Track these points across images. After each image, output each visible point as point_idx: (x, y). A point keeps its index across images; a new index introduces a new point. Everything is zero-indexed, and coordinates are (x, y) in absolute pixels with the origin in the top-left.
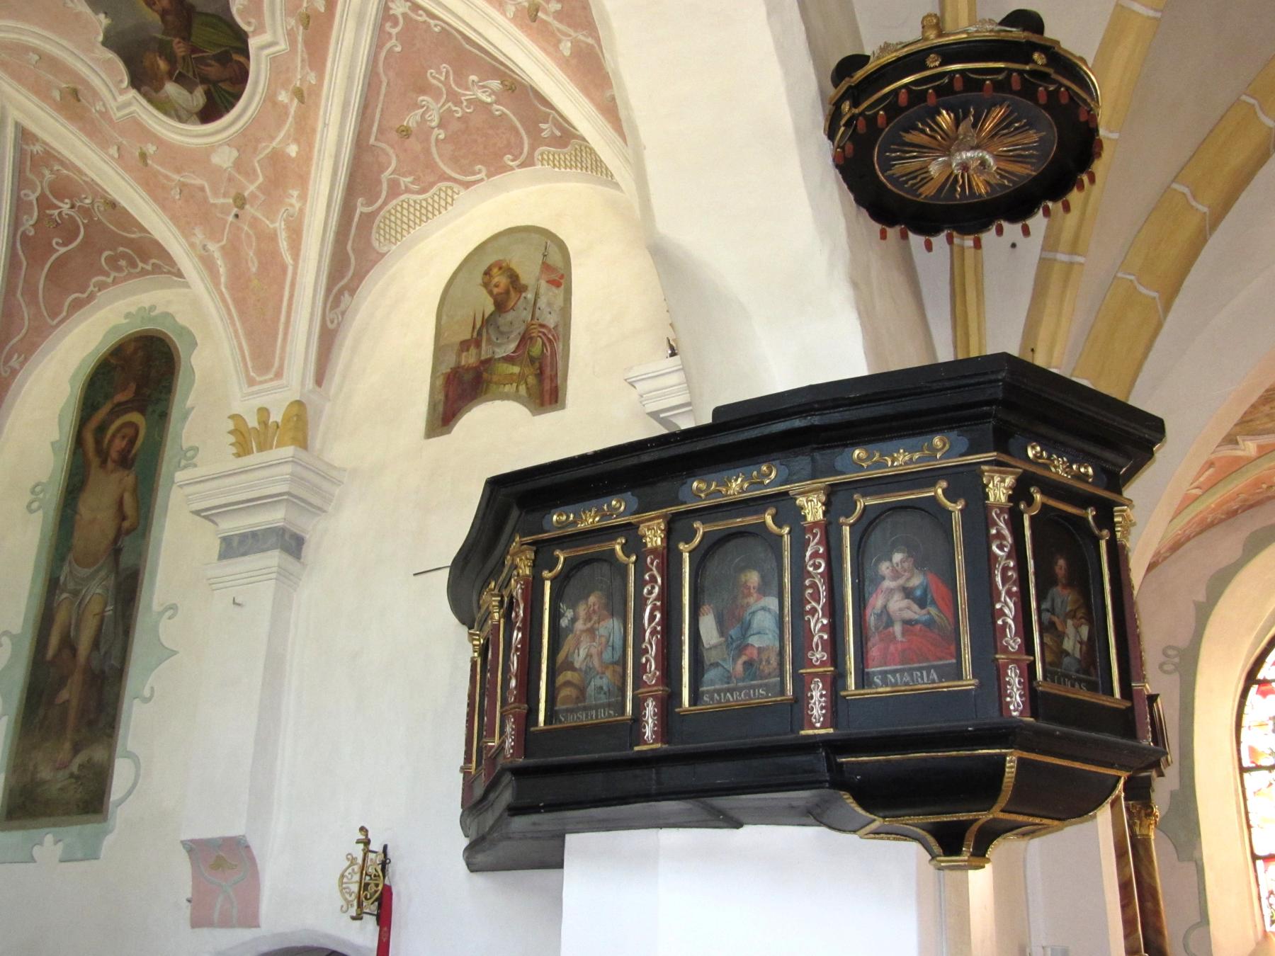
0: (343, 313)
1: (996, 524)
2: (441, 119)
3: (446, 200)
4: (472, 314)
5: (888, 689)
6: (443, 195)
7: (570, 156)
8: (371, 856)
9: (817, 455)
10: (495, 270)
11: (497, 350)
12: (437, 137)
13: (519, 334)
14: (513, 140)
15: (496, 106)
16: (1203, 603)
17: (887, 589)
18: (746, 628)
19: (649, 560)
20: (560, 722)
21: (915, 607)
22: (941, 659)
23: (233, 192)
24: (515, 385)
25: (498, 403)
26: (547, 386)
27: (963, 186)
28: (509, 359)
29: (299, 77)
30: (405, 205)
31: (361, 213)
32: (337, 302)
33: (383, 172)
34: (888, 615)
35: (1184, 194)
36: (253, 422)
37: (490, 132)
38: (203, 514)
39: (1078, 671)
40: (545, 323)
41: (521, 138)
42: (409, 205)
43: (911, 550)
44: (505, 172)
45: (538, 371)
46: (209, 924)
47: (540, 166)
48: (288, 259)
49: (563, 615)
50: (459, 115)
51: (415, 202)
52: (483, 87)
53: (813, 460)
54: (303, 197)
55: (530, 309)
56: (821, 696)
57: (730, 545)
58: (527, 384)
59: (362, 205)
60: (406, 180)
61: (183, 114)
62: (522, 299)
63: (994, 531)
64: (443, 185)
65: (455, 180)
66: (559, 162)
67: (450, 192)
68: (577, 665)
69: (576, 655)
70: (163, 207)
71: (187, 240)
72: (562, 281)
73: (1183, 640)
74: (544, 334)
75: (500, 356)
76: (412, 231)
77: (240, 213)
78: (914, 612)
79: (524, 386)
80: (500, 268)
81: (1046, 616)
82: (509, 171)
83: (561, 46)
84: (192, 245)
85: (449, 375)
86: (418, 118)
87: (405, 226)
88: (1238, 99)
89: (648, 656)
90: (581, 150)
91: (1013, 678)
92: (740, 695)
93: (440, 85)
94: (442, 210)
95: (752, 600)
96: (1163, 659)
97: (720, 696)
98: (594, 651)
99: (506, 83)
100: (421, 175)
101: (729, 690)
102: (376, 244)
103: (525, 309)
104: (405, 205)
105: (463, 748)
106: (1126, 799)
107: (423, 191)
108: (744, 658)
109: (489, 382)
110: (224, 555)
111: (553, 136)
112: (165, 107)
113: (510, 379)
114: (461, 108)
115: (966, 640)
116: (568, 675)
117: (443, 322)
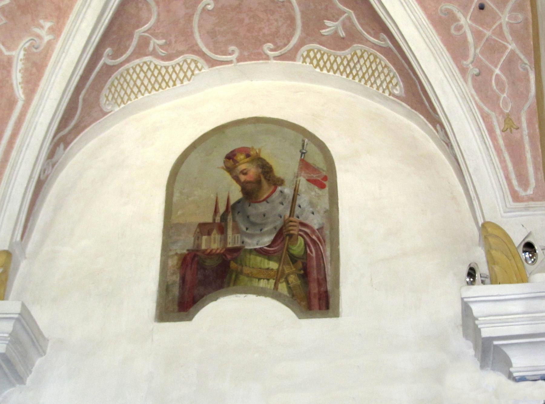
4: (213, 196)
6: (185, 67)
11: (247, 240)
12: (206, 5)
13: (275, 228)
14: (283, 30)
25: (251, 297)
26: (314, 289)
28: (261, 252)
30: (145, 68)
33: (138, 27)
41: (294, 30)
44: (258, 60)
45: (302, 272)
47: (301, 63)
48: (20, 93)
51: (156, 66)
54: (56, 31)
60: (155, 42)
62: (277, 194)
64: (190, 57)
67: (193, 66)
75: (252, 247)
76: (140, 97)
79: (284, 285)
80: (248, 156)
82: (265, 59)
87: (136, 90)
100: (173, 41)
102: (103, 100)
103: (282, 204)
104: (145, 68)
107: (169, 58)
109: (239, 273)
113: (267, 274)
117: (175, 199)
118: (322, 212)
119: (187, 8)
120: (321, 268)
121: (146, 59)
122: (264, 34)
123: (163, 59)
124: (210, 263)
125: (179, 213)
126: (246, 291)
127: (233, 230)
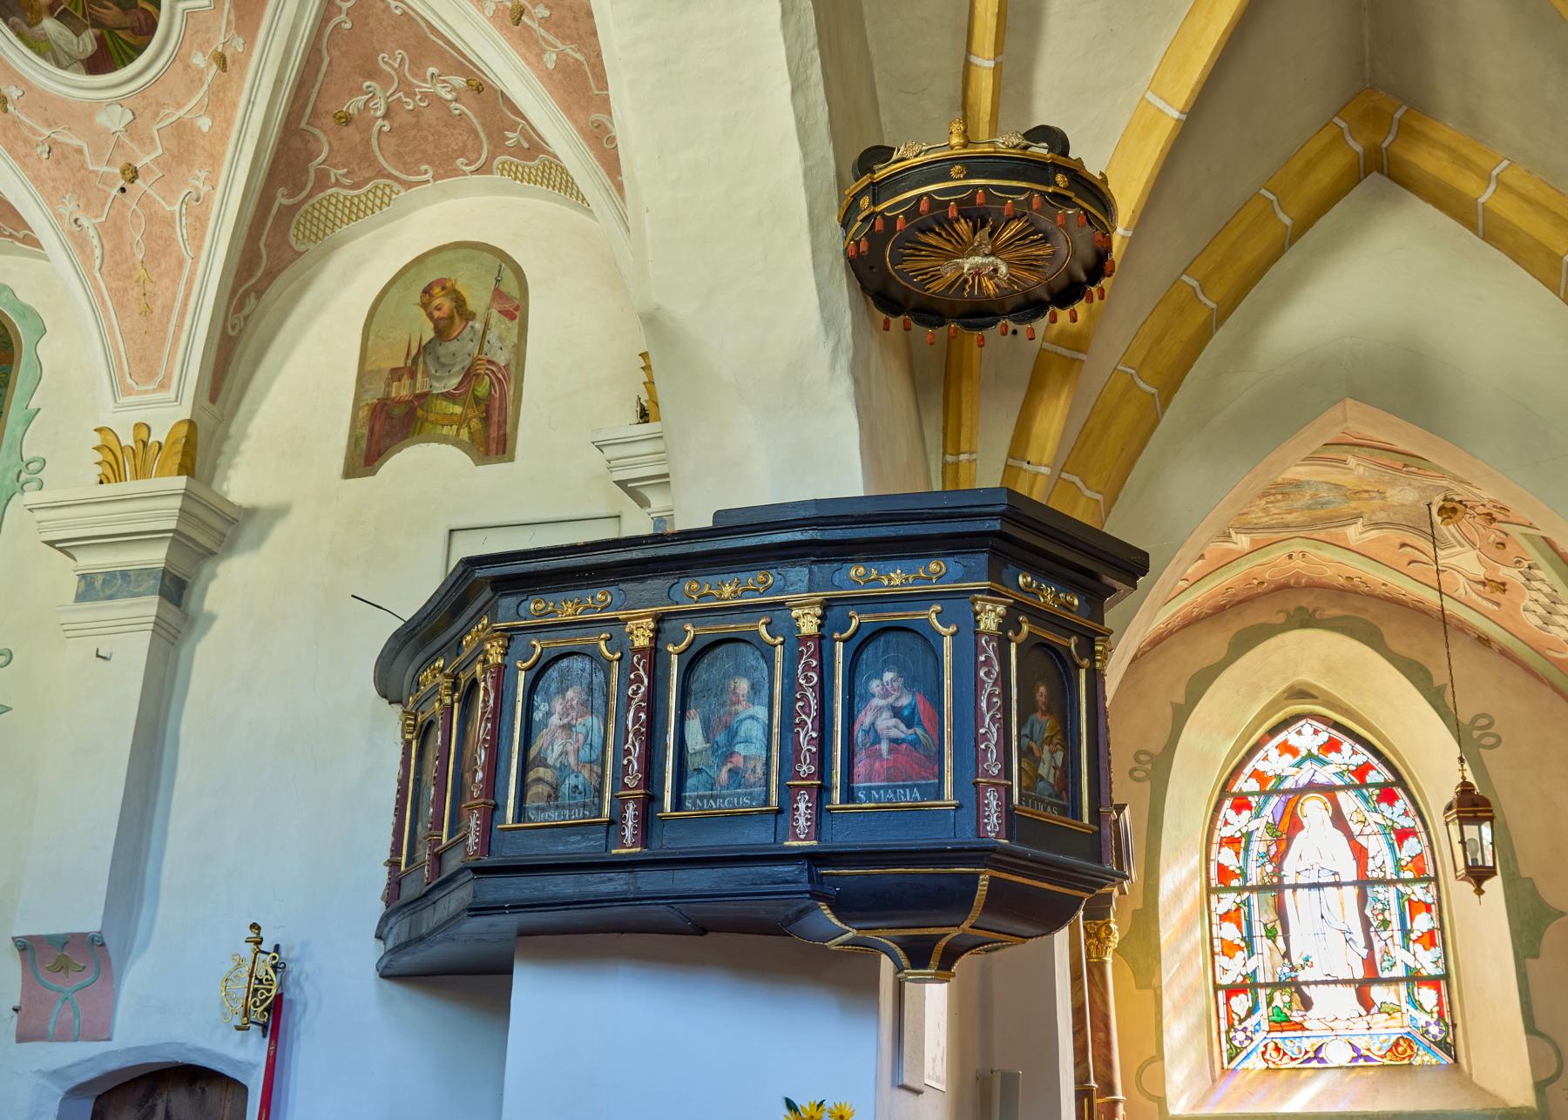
0: (246, 318)
1: (986, 652)
2: (388, 109)
3: (382, 199)
4: (407, 337)
5: (872, 805)
6: (379, 193)
7: (537, 171)
8: (261, 956)
9: (815, 568)
10: (437, 290)
11: (436, 384)
13: (463, 368)
14: (470, 144)
15: (454, 105)
16: (1181, 705)
17: (876, 707)
18: (732, 734)
19: (635, 659)
20: (530, 820)
21: (903, 727)
22: (923, 778)
23: (121, 162)
24: (455, 427)
25: (434, 445)
26: (494, 433)
27: (972, 286)
28: (448, 396)
29: (222, 40)
31: (281, 204)
32: (241, 306)
34: (876, 731)
35: (1193, 288)
36: (127, 439)
37: (445, 130)
38: (57, 545)
39: (1050, 796)
40: (494, 359)
41: (481, 142)
42: (338, 200)
43: (902, 670)
46: (42, 1037)
48: (188, 254)
49: (538, 708)
50: (411, 107)
52: (444, 81)
53: (811, 572)
55: (477, 342)
56: (807, 808)
57: (719, 651)
58: (470, 428)
59: (283, 195)
61: (63, 59)
63: (982, 658)
64: (381, 181)
65: (396, 179)
66: (522, 174)
67: (387, 191)
68: (550, 762)
69: (549, 752)
70: (24, 165)
71: (53, 210)
72: (517, 313)
73: (1156, 744)
74: (493, 372)
77: (128, 186)
78: (901, 731)
80: (444, 288)
81: (1025, 741)
82: (463, 175)
83: (546, 57)
84: (59, 216)
85: (375, 407)
86: (361, 105)
88: (1258, 192)
89: (631, 758)
90: (551, 168)
91: (992, 799)
92: (723, 803)
93: (393, 73)
94: (376, 209)
95: (740, 708)
96: (1135, 765)
97: (702, 802)
98: (570, 748)
99: (473, 83)
100: (357, 169)
101: (712, 797)
102: (293, 240)
104: (333, 200)
105: (389, 839)
106: (1084, 919)
108: (729, 766)
110: (81, 597)
111: (518, 145)
112: (41, 47)
113: (450, 419)
114: (414, 100)
115: (948, 763)
116: (541, 772)
118: (510, 347)
119: (361, 133)
120: (503, 409)
121: (330, 191)
122: (453, 149)
123: (352, 187)
124: (397, 412)
125: (373, 358)
126: (430, 440)
127: (423, 373)
